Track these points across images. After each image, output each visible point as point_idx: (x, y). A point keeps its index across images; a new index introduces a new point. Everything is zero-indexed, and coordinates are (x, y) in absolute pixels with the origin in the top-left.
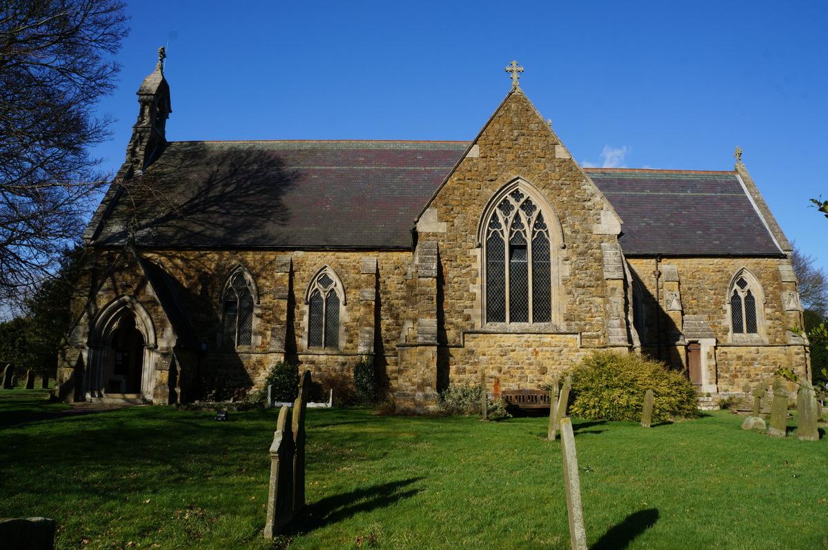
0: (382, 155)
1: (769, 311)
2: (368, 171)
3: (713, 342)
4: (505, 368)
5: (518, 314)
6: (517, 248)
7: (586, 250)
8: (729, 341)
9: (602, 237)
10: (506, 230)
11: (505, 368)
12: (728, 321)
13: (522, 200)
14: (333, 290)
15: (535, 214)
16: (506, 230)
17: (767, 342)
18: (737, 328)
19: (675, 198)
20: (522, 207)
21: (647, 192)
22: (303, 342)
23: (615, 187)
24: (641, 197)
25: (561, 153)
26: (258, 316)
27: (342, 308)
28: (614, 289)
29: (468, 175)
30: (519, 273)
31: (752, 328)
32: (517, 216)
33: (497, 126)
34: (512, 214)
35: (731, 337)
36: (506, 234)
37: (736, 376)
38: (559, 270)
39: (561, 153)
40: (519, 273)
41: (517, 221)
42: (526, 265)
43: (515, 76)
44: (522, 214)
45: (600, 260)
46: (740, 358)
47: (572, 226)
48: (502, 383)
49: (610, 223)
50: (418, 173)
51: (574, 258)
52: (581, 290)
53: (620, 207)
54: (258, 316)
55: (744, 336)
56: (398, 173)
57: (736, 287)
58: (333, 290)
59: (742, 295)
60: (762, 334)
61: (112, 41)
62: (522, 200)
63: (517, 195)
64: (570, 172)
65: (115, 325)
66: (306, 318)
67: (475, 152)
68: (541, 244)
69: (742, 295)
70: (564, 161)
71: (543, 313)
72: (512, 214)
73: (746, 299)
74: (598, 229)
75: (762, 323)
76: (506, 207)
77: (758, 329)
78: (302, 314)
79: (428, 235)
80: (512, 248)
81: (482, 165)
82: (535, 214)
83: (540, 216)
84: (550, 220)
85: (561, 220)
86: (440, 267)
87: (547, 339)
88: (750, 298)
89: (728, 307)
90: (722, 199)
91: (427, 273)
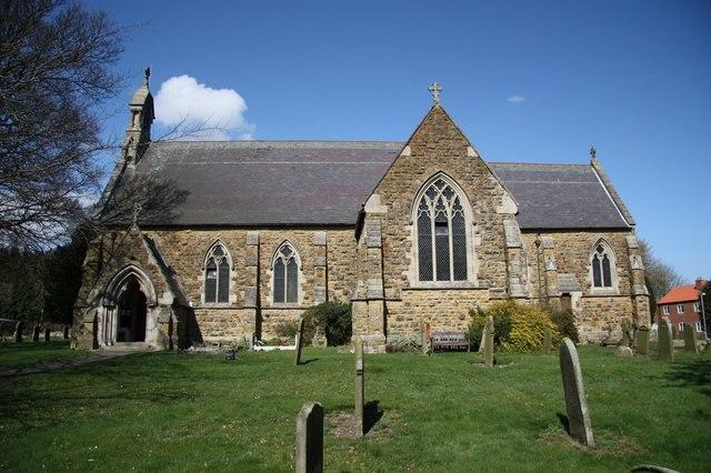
0: (324, 153)
1: (620, 270)
2: (315, 165)
3: (580, 294)
4: (434, 316)
5: (443, 275)
6: (441, 224)
7: (492, 225)
8: (592, 293)
9: (504, 216)
10: (449, 210)
11: (434, 316)
12: (590, 278)
13: (444, 188)
14: (292, 258)
15: (453, 199)
16: (449, 210)
17: (619, 293)
18: (598, 284)
19: (548, 186)
20: (444, 193)
21: (528, 181)
22: (269, 299)
23: (518, 182)
24: (523, 185)
25: (471, 152)
26: (234, 279)
27: (300, 273)
28: (513, 255)
29: (402, 169)
30: (442, 242)
31: (608, 283)
32: (440, 200)
33: (423, 132)
34: (436, 198)
35: (594, 290)
36: (432, 213)
37: (596, 319)
38: (473, 240)
39: (471, 152)
40: (442, 242)
41: (440, 205)
42: (447, 237)
43: (436, 94)
44: (444, 198)
45: (503, 234)
46: (599, 306)
47: (481, 208)
48: (432, 327)
49: (509, 206)
50: (354, 166)
51: (483, 232)
52: (489, 256)
53: (518, 194)
54: (234, 279)
55: (603, 289)
56: (338, 167)
57: (281, 255)
58: (292, 258)
59: (601, 259)
60: (615, 288)
61: (113, 54)
62: (444, 188)
63: (440, 184)
64: (481, 168)
65: (124, 288)
66: (272, 280)
67: (407, 152)
68: (459, 220)
69: (601, 259)
70: (474, 158)
71: (461, 273)
72: (436, 198)
73: (221, 265)
74: (500, 210)
75: (616, 281)
76: (431, 193)
77: (613, 283)
78: (269, 277)
79: (372, 215)
80: (437, 224)
81: (413, 160)
82: (453, 199)
83: (457, 200)
84: (465, 203)
85: (473, 203)
86: (383, 239)
87: (465, 293)
88: (606, 261)
89: (591, 268)
90: (584, 186)
91: (374, 244)
